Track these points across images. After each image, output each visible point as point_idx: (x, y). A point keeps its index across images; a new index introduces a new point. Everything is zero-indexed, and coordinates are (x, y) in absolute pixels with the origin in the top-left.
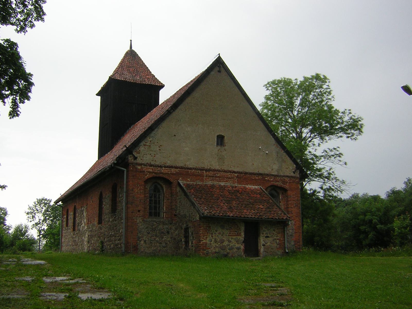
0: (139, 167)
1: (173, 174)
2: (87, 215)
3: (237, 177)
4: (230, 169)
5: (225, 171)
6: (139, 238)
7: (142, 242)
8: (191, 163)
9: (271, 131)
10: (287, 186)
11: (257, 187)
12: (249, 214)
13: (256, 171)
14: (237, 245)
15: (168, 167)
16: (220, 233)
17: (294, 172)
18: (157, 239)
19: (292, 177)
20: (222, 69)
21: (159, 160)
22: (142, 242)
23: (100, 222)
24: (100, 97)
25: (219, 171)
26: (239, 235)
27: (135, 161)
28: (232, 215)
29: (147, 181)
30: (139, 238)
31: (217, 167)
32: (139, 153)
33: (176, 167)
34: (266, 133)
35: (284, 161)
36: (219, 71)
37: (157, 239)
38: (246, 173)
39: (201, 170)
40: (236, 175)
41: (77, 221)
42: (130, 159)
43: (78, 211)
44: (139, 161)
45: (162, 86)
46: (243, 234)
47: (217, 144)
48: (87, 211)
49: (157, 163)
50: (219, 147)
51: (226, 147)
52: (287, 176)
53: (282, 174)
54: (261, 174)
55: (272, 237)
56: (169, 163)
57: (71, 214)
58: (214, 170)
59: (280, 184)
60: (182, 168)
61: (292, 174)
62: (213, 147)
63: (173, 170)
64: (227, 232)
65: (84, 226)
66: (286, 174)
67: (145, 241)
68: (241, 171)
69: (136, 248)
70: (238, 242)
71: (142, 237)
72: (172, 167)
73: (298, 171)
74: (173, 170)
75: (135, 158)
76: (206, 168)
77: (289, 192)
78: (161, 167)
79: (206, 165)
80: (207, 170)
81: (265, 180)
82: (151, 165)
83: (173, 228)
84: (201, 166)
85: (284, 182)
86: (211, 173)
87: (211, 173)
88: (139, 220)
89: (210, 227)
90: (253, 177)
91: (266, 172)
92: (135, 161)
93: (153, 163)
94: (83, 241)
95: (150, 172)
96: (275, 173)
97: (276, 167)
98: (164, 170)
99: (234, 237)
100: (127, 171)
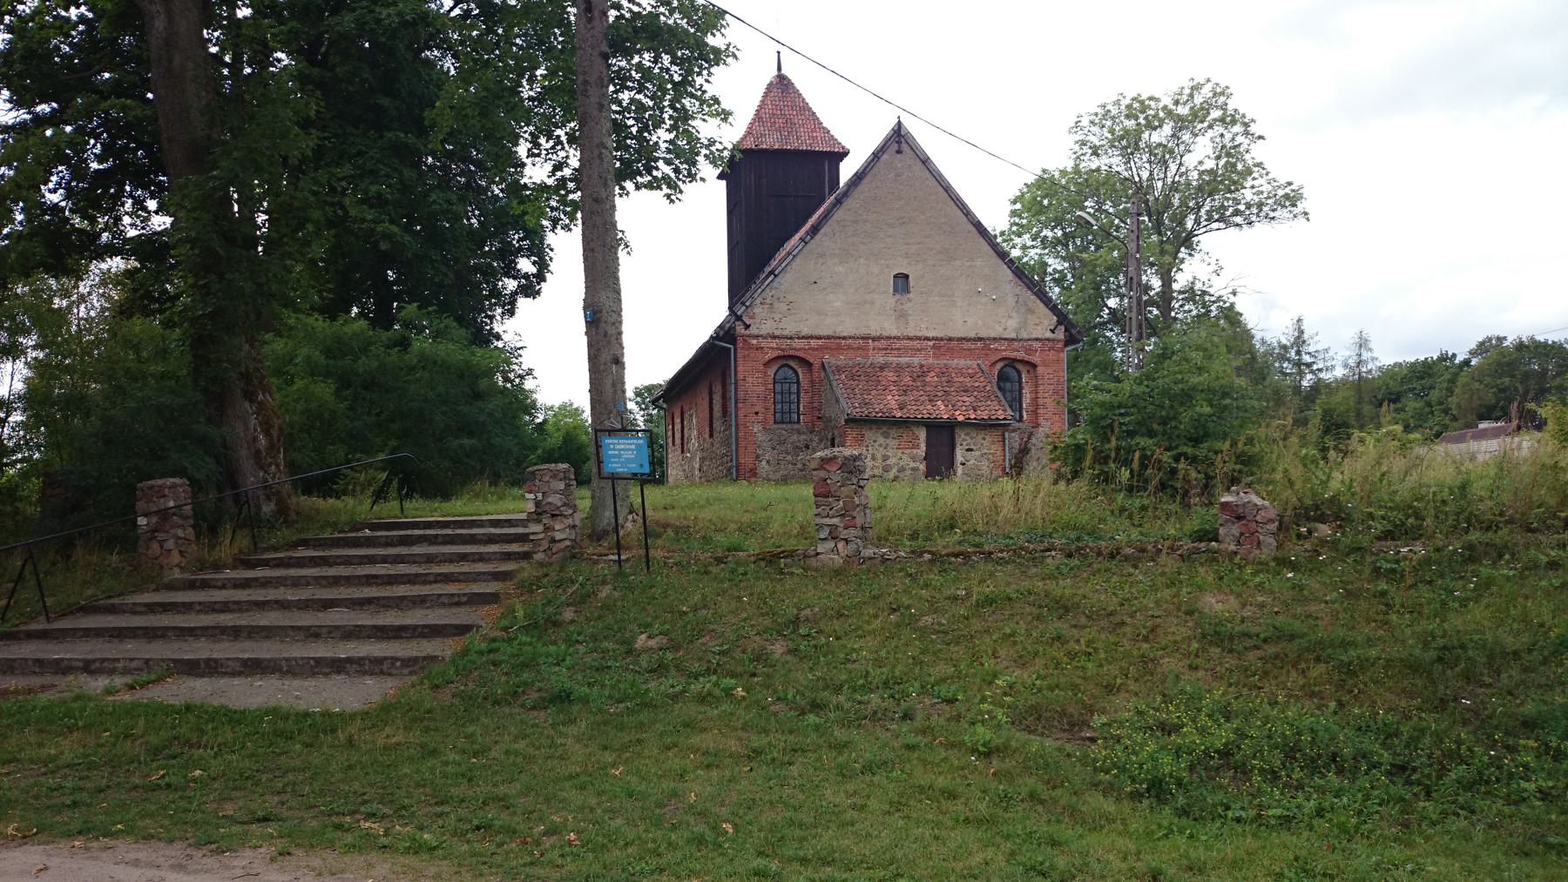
0: (755, 342)
1: (813, 349)
2: (698, 422)
3: (934, 347)
4: (919, 334)
5: (909, 338)
6: (758, 457)
7: (764, 463)
8: (847, 327)
9: (1003, 255)
10: (1036, 359)
11: (969, 363)
12: (942, 411)
13: (972, 335)
14: (912, 465)
15: (803, 337)
16: (881, 445)
17: (1053, 331)
18: (789, 458)
19: (1048, 340)
20: (904, 146)
21: (790, 327)
22: (764, 463)
23: (711, 436)
24: (724, 183)
25: (897, 338)
26: (917, 447)
27: (747, 332)
28: (899, 415)
29: (768, 364)
30: (758, 457)
31: (895, 333)
32: (752, 318)
33: (819, 338)
34: (996, 259)
35: (1031, 311)
36: (899, 152)
37: (789, 458)
38: (950, 339)
39: (863, 338)
40: (931, 343)
41: (686, 435)
42: (740, 329)
43: (686, 415)
44: (753, 330)
45: (845, 154)
46: (923, 447)
47: (895, 290)
48: (697, 417)
49: (786, 333)
50: (898, 296)
51: (911, 295)
52: (1037, 339)
53: (1026, 337)
54: (980, 339)
55: (979, 449)
56: (806, 331)
57: (678, 420)
58: (889, 338)
59: (1021, 355)
60: (828, 338)
61: (1049, 335)
62: (889, 300)
63: (813, 343)
64: (893, 443)
65: (694, 444)
66: (1034, 336)
67: (768, 462)
68: (940, 335)
69: (753, 473)
70: (914, 459)
71: (764, 455)
72: (811, 337)
73: (1062, 328)
74: (813, 343)
75: (747, 327)
76: (873, 334)
77: (1040, 369)
78: (791, 338)
79: (874, 331)
80: (874, 339)
81: (990, 349)
82: (774, 337)
83: (816, 439)
84: (863, 331)
85: (1029, 351)
86: (882, 344)
87: (882, 344)
88: (757, 428)
89: (863, 436)
90: (966, 345)
91: (993, 335)
92: (747, 332)
93: (777, 333)
94: (693, 468)
95: (772, 348)
96: (1013, 335)
97: (1012, 323)
98: (797, 344)
99: (907, 451)
100: (735, 350)
